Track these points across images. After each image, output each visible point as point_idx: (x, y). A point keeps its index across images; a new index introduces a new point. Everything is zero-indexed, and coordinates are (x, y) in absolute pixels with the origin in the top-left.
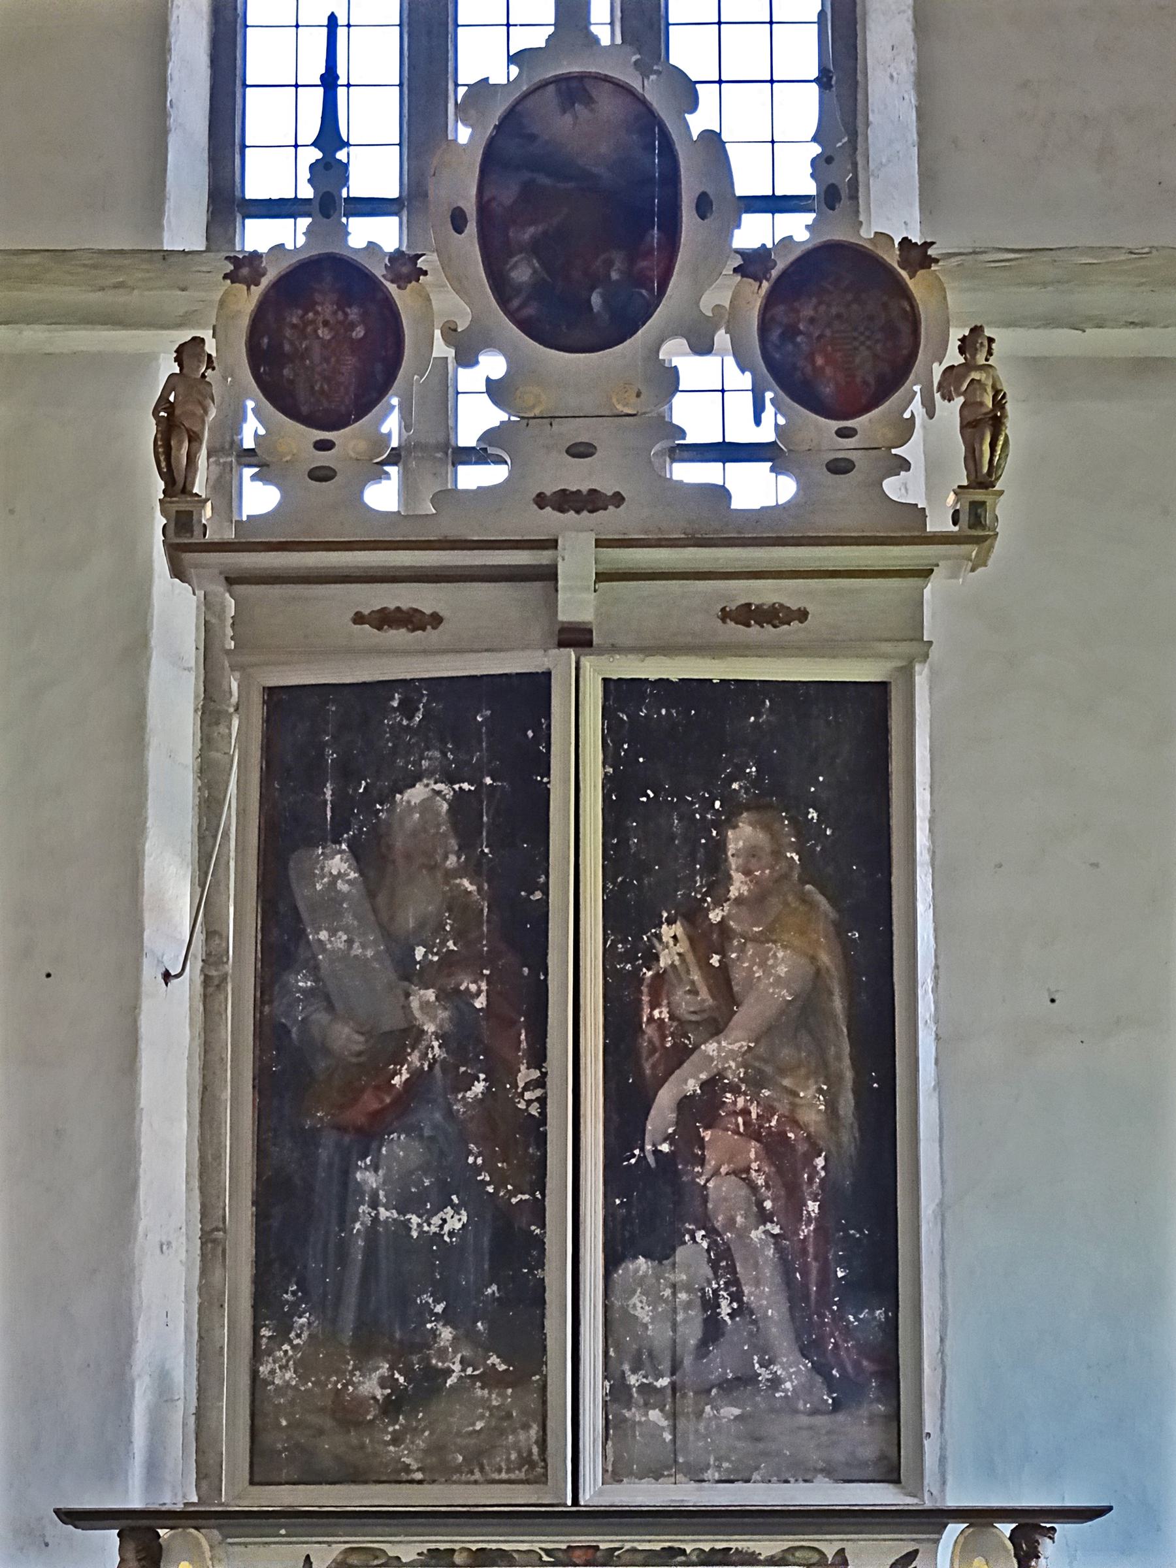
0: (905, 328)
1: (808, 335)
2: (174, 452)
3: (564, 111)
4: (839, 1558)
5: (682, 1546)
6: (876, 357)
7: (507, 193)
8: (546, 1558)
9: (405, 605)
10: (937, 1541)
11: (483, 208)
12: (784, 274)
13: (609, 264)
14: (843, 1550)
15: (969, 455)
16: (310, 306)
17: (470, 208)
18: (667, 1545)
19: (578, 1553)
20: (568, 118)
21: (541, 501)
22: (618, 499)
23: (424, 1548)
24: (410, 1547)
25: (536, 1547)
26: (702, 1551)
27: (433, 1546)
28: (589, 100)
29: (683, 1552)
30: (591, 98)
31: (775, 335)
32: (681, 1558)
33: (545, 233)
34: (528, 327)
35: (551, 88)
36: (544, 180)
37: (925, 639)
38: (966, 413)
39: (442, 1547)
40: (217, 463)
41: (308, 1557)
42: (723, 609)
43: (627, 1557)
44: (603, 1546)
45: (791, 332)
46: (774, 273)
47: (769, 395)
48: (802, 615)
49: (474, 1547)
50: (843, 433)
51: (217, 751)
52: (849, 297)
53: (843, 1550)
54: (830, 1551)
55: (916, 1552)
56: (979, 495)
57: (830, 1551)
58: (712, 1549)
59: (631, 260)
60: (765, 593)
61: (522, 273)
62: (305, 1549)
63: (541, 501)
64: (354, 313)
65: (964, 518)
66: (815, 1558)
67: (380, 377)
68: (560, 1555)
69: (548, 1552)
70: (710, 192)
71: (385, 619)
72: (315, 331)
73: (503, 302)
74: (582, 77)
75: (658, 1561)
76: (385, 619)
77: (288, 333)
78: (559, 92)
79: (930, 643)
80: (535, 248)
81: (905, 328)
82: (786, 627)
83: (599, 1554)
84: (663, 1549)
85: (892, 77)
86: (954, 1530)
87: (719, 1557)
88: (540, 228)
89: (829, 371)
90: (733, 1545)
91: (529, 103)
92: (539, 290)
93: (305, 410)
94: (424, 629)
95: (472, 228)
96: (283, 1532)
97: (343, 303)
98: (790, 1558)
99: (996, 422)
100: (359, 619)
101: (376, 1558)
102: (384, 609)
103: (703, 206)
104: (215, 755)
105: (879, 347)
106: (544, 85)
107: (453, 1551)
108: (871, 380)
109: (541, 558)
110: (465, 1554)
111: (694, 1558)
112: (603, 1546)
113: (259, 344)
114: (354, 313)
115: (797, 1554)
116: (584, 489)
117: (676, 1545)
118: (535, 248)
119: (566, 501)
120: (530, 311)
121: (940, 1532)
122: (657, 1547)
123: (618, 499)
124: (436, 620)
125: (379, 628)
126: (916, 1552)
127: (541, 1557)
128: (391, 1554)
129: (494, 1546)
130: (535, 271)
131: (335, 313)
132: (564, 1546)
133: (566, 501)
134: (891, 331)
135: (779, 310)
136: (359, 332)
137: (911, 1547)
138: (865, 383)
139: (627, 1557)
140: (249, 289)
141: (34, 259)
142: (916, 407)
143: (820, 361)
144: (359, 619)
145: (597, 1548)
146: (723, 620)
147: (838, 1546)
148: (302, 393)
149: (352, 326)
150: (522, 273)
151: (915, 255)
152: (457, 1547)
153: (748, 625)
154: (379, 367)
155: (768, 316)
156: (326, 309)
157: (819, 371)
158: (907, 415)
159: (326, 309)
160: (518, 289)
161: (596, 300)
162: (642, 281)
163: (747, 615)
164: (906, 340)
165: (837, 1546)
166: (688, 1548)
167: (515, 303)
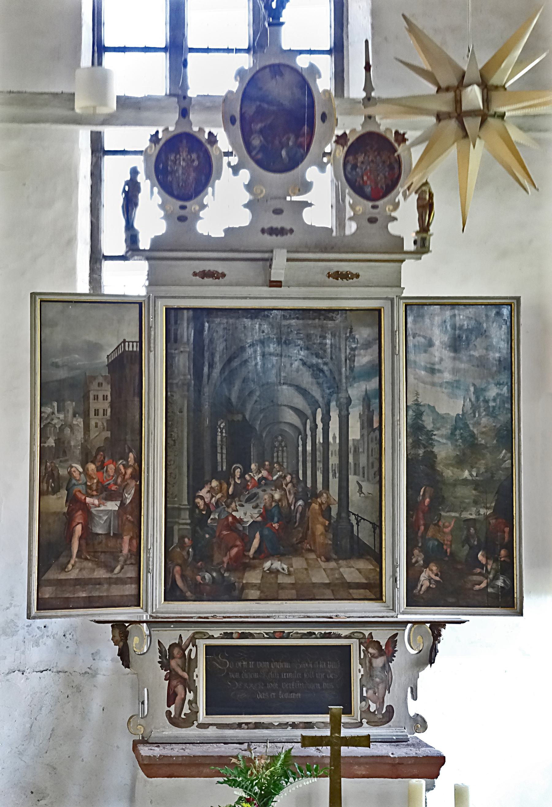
0: (396, 166)
1: (361, 168)
2: (130, 212)
3: (272, 78)
4: (370, 636)
5: (314, 631)
6: (385, 177)
7: (251, 110)
8: (266, 636)
9: (212, 269)
10: (404, 630)
11: (242, 115)
12: (352, 144)
13: (288, 139)
14: (371, 633)
15: (421, 218)
16: (178, 152)
17: (238, 116)
18: (309, 631)
19: (277, 634)
20: (274, 82)
21: (263, 231)
22: (291, 231)
23: (222, 632)
24: (216, 632)
25: (262, 632)
26: (321, 633)
27: (225, 631)
28: (281, 74)
29: (314, 634)
30: (281, 72)
31: (349, 167)
32: (314, 636)
33: (265, 126)
34: (259, 163)
35: (268, 70)
36: (265, 106)
37: (402, 286)
38: (420, 201)
39: (229, 632)
40: (95, 156)
41: (180, 635)
42: (329, 273)
43: (295, 635)
44: (286, 631)
45: (355, 167)
46: (349, 143)
47: (347, 191)
48: (358, 276)
49: (240, 632)
50: (374, 207)
51: (96, 274)
52: (376, 153)
53: (371, 633)
54: (367, 634)
55: (397, 634)
56: (424, 235)
57: (367, 634)
58: (325, 633)
59: (297, 137)
60: (344, 267)
61: (256, 142)
62: (179, 633)
63: (263, 231)
64: (194, 156)
65: (419, 242)
66: (362, 636)
67: (203, 181)
68: (271, 635)
69: (267, 634)
70: (327, 112)
71: (204, 274)
72: (180, 162)
73: (249, 152)
74: (279, 65)
75: (306, 637)
76: (204, 274)
77: (170, 163)
78: (270, 70)
79: (404, 288)
80: (261, 132)
81: (396, 166)
82: (351, 280)
83: (284, 634)
84: (308, 633)
85: (360, 7)
86: (409, 625)
87: (328, 635)
88: (263, 125)
89: (368, 182)
90: (332, 631)
91: (259, 75)
92: (263, 148)
93: (176, 193)
94: (219, 279)
95: (238, 123)
96: (172, 626)
97: (190, 152)
98: (352, 636)
99: (431, 206)
100: (195, 274)
101: (205, 635)
102: (204, 271)
103: (324, 117)
104: (95, 276)
105: (387, 174)
106: (264, 68)
107: (232, 633)
108: (384, 186)
109: (266, 255)
110: (237, 634)
111: (318, 636)
112: (286, 631)
113: (159, 167)
114: (194, 156)
115: (355, 634)
116: (279, 227)
117: (312, 631)
118: (261, 132)
119: (273, 231)
120: (260, 156)
121: (406, 627)
122: (306, 632)
123: (291, 231)
124: (223, 275)
125: (203, 278)
126: (397, 634)
127: (264, 636)
128: (210, 634)
129: (247, 631)
130: (261, 141)
131: (187, 156)
132: (272, 631)
133: (273, 231)
134: (391, 167)
135: (351, 158)
136: (196, 163)
137: (395, 632)
138: (382, 187)
139: (295, 635)
140: (155, 145)
141: (46, 96)
142: (400, 197)
143: (365, 178)
144: (195, 274)
145: (284, 632)
146: (329, 277)
147: (369, 632)
148: (175, 186)
149: (194, 161)
150: (256, 142)
151: (400, 138)
152: (234, 631)
153: (338, 279)
154: (203, 178)
155: (347, 159)
156: (184, 154)
157: (365, 183)
158: (397, 200)
159: (184, 154)
160: (255, 148)
161: (284, 153)
162: (301, 146)
163: (338, 275)
164: (396, 170)
165: (369, 632)
166: (316, 632)
167: (254, 153)
